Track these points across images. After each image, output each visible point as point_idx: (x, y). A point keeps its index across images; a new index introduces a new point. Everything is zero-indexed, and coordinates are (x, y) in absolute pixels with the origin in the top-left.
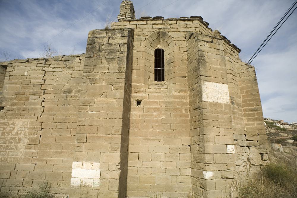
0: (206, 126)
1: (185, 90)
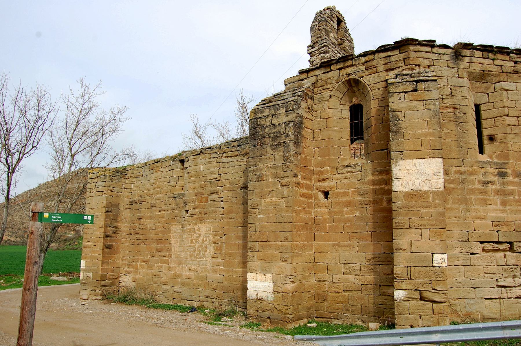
0: (398, 227)
1: (386, 171)
